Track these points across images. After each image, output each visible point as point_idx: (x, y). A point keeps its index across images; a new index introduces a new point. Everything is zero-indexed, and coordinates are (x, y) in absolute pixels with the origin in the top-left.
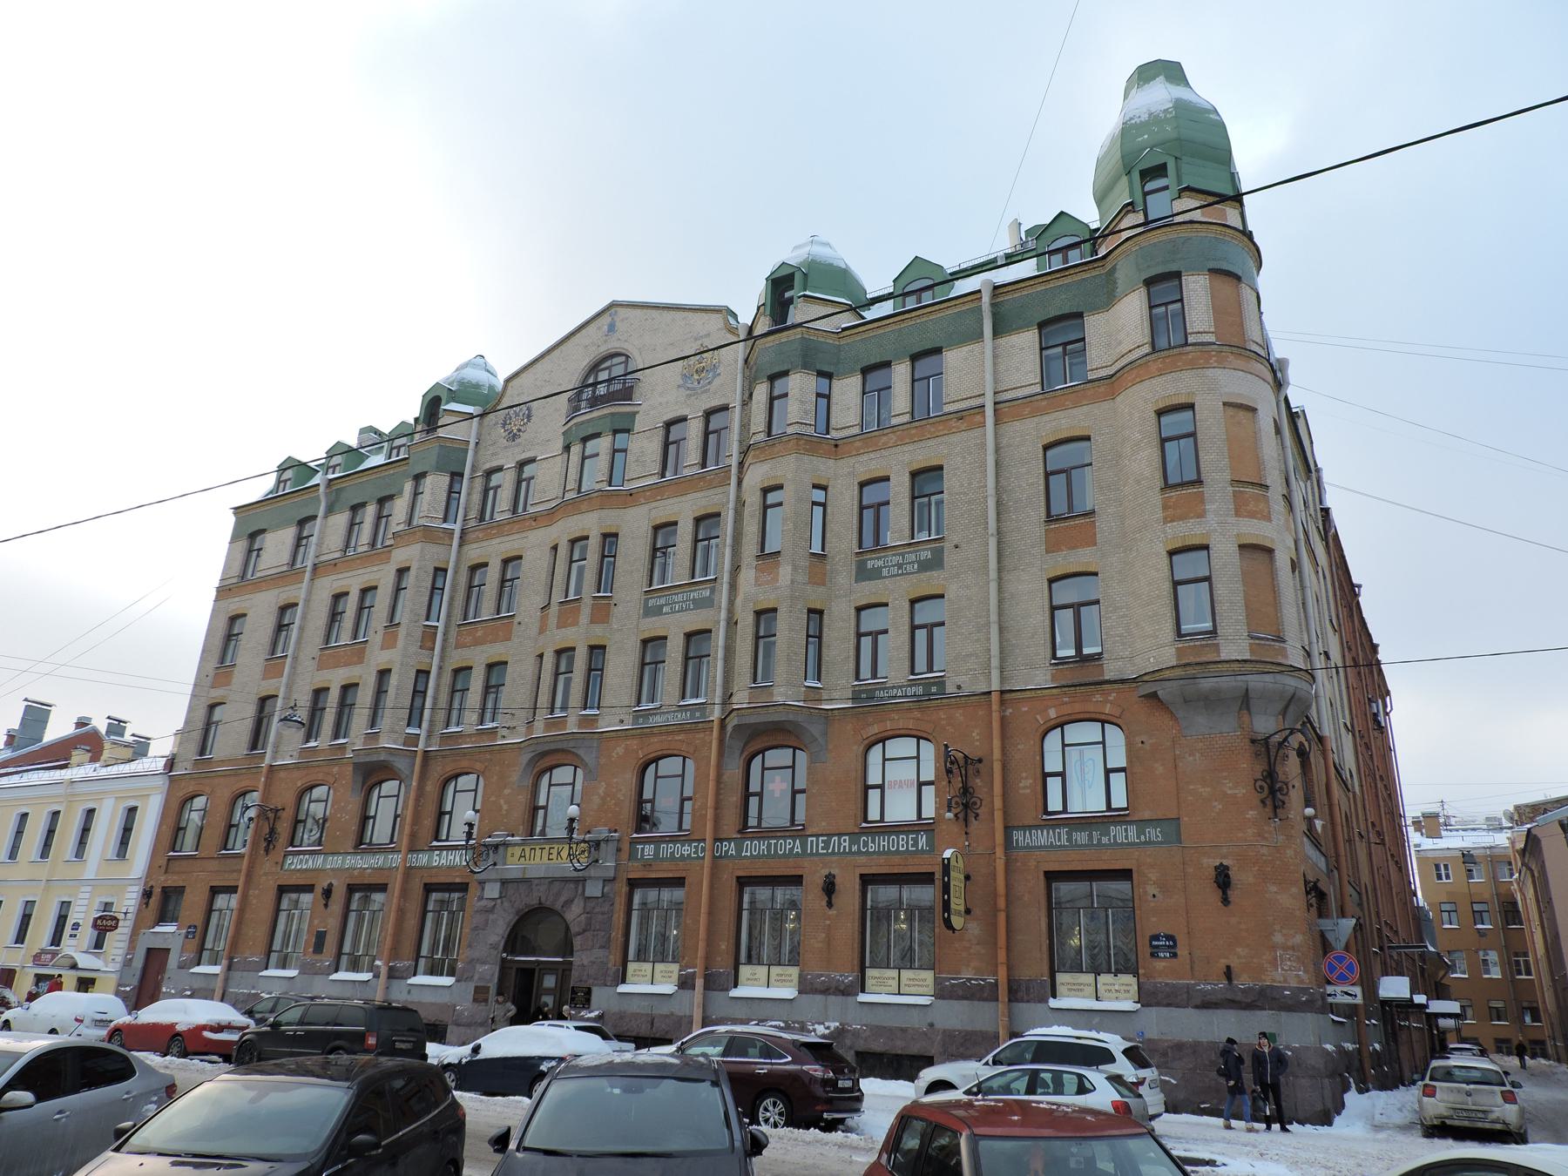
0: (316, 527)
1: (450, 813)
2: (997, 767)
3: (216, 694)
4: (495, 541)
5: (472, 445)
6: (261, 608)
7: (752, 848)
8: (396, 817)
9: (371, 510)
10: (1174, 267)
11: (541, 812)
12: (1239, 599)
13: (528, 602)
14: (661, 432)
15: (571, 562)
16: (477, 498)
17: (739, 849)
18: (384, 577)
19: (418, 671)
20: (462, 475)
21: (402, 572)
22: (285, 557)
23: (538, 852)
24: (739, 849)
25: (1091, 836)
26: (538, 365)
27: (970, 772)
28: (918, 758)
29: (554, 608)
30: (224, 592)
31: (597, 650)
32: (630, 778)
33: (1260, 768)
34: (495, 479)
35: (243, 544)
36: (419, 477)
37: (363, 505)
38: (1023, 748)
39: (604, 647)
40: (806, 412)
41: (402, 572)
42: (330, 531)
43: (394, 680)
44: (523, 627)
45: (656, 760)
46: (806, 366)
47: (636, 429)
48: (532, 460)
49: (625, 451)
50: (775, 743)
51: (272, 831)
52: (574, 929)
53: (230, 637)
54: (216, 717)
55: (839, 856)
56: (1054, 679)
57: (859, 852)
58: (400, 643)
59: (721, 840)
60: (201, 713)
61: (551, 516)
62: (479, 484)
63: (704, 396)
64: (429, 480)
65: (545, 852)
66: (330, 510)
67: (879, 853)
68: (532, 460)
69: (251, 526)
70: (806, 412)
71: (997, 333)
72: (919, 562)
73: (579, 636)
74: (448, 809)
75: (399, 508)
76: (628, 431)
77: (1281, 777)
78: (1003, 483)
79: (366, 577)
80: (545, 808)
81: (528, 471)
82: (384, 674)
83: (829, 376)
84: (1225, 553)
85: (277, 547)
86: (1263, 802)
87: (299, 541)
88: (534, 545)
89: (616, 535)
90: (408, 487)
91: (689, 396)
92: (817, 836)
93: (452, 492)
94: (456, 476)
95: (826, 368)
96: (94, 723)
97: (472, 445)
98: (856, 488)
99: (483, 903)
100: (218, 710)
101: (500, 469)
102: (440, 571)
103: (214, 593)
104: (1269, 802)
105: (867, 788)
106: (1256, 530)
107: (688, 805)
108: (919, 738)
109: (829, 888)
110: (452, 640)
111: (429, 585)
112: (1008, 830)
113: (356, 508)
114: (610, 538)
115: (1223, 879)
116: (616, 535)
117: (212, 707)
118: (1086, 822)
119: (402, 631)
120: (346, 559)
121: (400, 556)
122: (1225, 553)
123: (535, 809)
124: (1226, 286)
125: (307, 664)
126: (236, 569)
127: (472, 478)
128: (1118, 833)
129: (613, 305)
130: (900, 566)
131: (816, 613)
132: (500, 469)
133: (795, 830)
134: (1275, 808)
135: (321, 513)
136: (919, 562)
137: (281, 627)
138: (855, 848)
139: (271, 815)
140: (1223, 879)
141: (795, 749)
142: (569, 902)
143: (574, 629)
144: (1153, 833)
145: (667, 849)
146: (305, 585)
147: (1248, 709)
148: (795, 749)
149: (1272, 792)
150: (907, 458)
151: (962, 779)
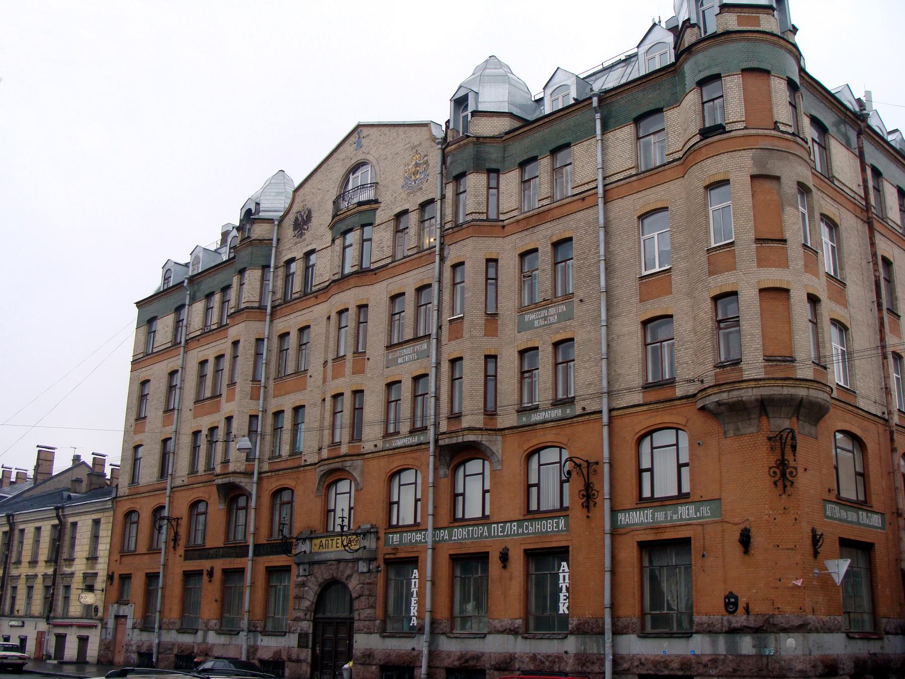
0: (185, 313)
1: (398, 503)
2: (606, 468)
3: (137, 439)
4: (292, 316)
5: (274, 242)
6: (158, 372)
7: (459, 533)
8: (417, 501)
9: (217, 297)
10: (714, 71)
11: (534, 490)
12: (758, 331)
13: (315, 362)
14: (392, 224)
15: (340, 328)
16: (280, 283)
17: (450, 536)
18: (225, 346)
19: (251, 416)
20: (269, 267)
21: (236, 343)
22: (169, 337)
23: (330, 542)
24: (450, 536)
25: (666, 514)
26: (314, 177)
27: (591, 471)
28: (677, 445)
29: (330, 364)
30: (135, 363)
31: (358, 393)
32: (381, 486)
33: (773, 459)
34: (293, 267)
35: (144, 329)
36: (242, 272)
37: (228, 287)
38: (626, 453)
39: (362, 391)
40: (479, 204)
41: (236, 343)
42: (195, 315)
43: (235, 424)
44: (312, 379)
45: (650, 433)
46: (477, 169)
47: (377, 222)
48: (313, 251)
49: (370, 240)
50: (469, 457)
51: (176, 534)
52: (354, 595)
53: (143, 397)
54: (140, 455)
55: (516, 535)
56: (485, 424)
57: (523, 533)
58: (237, 396)
59: (440, 529)
60: (130, 453)
61: (326, 290)
62: (281, 272)
63: (418, 194)
64: (247, 274)
65: (334, 542)
66: (193, 300)
67: (840, 520)
68: (313, 251)
69: (149, 310)
70: (479, 204)
71: (605, 129)
72: (559, 315)
73: (345, 384)
74: (395, 499)
75: (232, 294)
76: (371, 224)
77: (792, 463)
78: (612, 248)
79: (218, 348)
80: (537, 485)
81: (313, 258)
82: (229, 419)
83: (497, 171)
84: (749, 297)
85: (165, 326)
86: (775, 483)
87: (178, 322)
88: (317, 314)
89: (366, 306)
90: (235, 280)
91: (409, 194)
92: (497, 523)
93: (263, 279)
94: (265, 267)
95: (494, 166)
96: (83, 459)
97: (274, 242)
98: (517, 259)
99: (300, 579)
100: (141, 449)
101: (293, 260)
102: (259, 341)
103: (129, 367)
104: (780, 483)
105: (641, 471)
106: (773, 277)
107: (487, 495)
108: (677, 429)
109: (504, 557)
110: (271, 391)
111: (253, 352)
112: (614, 512)
113: (209, 296)
114: (362, 307)
115: (745, 540)
116: (366, 306)
117: (136, 447)
118: (664, 502)
119: (238, 388)
120: (207, 333)
121: (234, 332)
122: (749, 297)
123: (391, 504)
124: (755, 81)
125: (187, 414)
126: (141, 349)
127: (276, 268)
128: (686, 512)
129: (359, 126)
130: (545, 318)
131: (491, 358)
132: (293, 260)
133: (484, 520)
134: (785, 486)
135: (187, 302)
136: (559, 315)
137: (171, 388)
138: (520, 531)
139: (174, 523)
140: (745, 540)
141: (677, 429)
142: (350, 576)
143: (342, 379)
144: (705, 510)
145: (408, 537)
146: (181, 356)
147: (767, 415)
148: (561, 448)
149: (783, 475)
150: (549, 232)
151: (583, 475)
